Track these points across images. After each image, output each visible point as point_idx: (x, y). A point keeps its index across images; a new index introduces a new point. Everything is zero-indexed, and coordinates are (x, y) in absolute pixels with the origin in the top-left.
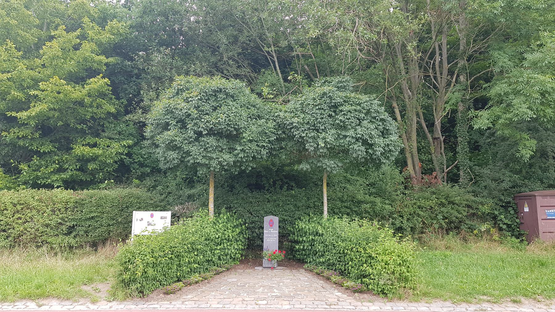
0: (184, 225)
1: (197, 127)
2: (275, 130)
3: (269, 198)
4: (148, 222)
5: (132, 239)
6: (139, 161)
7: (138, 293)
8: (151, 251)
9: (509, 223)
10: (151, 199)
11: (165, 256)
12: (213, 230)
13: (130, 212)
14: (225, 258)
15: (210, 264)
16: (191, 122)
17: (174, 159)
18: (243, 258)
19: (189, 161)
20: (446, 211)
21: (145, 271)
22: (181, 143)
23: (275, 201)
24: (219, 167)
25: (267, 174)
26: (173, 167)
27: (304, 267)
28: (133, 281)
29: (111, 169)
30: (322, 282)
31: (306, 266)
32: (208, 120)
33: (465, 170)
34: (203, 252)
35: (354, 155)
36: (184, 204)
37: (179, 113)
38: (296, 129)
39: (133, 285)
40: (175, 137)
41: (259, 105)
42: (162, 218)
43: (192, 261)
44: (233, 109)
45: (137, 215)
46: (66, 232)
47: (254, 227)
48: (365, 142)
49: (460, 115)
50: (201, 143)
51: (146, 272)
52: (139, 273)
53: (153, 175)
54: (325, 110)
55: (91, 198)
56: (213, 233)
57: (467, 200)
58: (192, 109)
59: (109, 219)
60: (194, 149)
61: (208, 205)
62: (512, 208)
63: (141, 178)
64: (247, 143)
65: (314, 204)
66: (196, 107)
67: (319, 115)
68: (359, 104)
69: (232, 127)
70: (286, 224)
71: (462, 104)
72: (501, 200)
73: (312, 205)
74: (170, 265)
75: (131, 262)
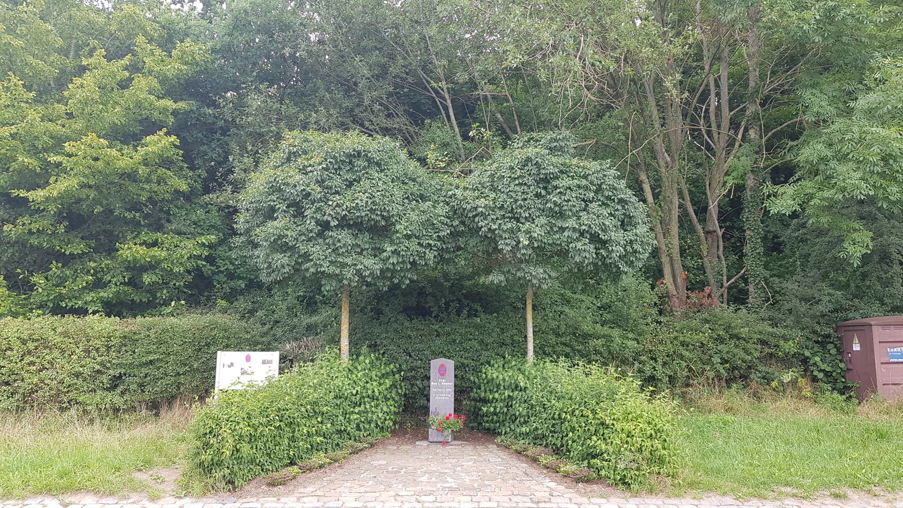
0: (301, 374)
1: (321, 213)
3: (439, 330)
4: (242, 369)
8: (247, 415)
10: (247, 332)
12: (347, 382)
13: (213, 354)
14: (367, 426)
15: (343, 437)
16: (311, 206)
17: (283, 267)
18: (397, 427)
19: (307, 270)
20: (726, 350)
21: (237, 449)
23: (449, 334)
26: (282, 279)
27: (496, 440)
28: (217, 464)
29: (182, 284)
30: (525, 465)
33: (758, 284)
34: (332, 418)
35: (577, 259)
36: (300, 339)
37: (292, 191)
38: (482, 218)
39: (218, 471)
40: (284, 231)
41: (422, 178)
42: (264, 362)
43: (314, 432)
45: (224, 358)
46: (109, 386)
47: (414, 377)
48: (595, 239)
50: (327, 241)
51: (238, 451)
52: (228, 452)
53: (250, 293)
54: (529, 187)
56: (347, 387)
58: (312, 184)
59: (177, 364)
60: (316, 250)
61: (339, 341)
63: (231, 297)
64: (403, 240)
66: (319, 182)
67: (520, 194)
68: (585, 177)
69: (377, 215)
70: (466, 371)
71: (752, 177)
72: (815, 332)
73: (508, 341)
74: (278, 438)
75: (213, 434)
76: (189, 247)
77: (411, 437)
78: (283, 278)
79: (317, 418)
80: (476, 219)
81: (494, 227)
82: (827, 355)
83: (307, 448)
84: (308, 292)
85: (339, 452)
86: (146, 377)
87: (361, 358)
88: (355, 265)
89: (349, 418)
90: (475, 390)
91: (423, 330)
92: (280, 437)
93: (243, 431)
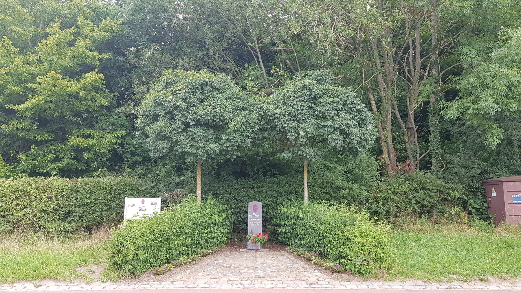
0: (173, 210)
1: (185, 118)
3: (254, 185)
4: (139, 208)
7: (130, 274)
8: (142, 234)
9: (478, 207)
10: (143, 186)
11: (155, 239)
14: (212, 241)
15: (198, 247)
17: (163, 149)
18: (229, 241)
19: (177, 150)
21: (136, 254)
22: (170, 133)
23: (259, 187)
26: (162, 155)
27: (286, 249)
28: (125, 263)
31: (288, 248)
32: (195, 111)
34: (191, 236)
36: (173, 191)
37: (168, 105)
38: (278, 120)
40: (164, 128)
43: (181, 244)
44: (219, 101)
45: (129, 201)
46: (62, 218)
48: (342, 132)
49: (432, 106)
50: (188, 133)
51: (137, 255)
52: (131, 256)
53: (144, 164)
54: (305, 102)
55: (85, 186)
57: (439, 186)
59: (102, 205)
60: (182, 139)
61: (195, 192)
63: (133, 166)
66: (184, 100)
70: (269, 209)
73: (293, 191)
74: (160, 248)
75: (123, 245)
78: (163, 155)
80: (275, 121)
81: (285, 125)
86: (84, 212)
87: (208, 201)
88: (205, 147)
93: (140, 243)
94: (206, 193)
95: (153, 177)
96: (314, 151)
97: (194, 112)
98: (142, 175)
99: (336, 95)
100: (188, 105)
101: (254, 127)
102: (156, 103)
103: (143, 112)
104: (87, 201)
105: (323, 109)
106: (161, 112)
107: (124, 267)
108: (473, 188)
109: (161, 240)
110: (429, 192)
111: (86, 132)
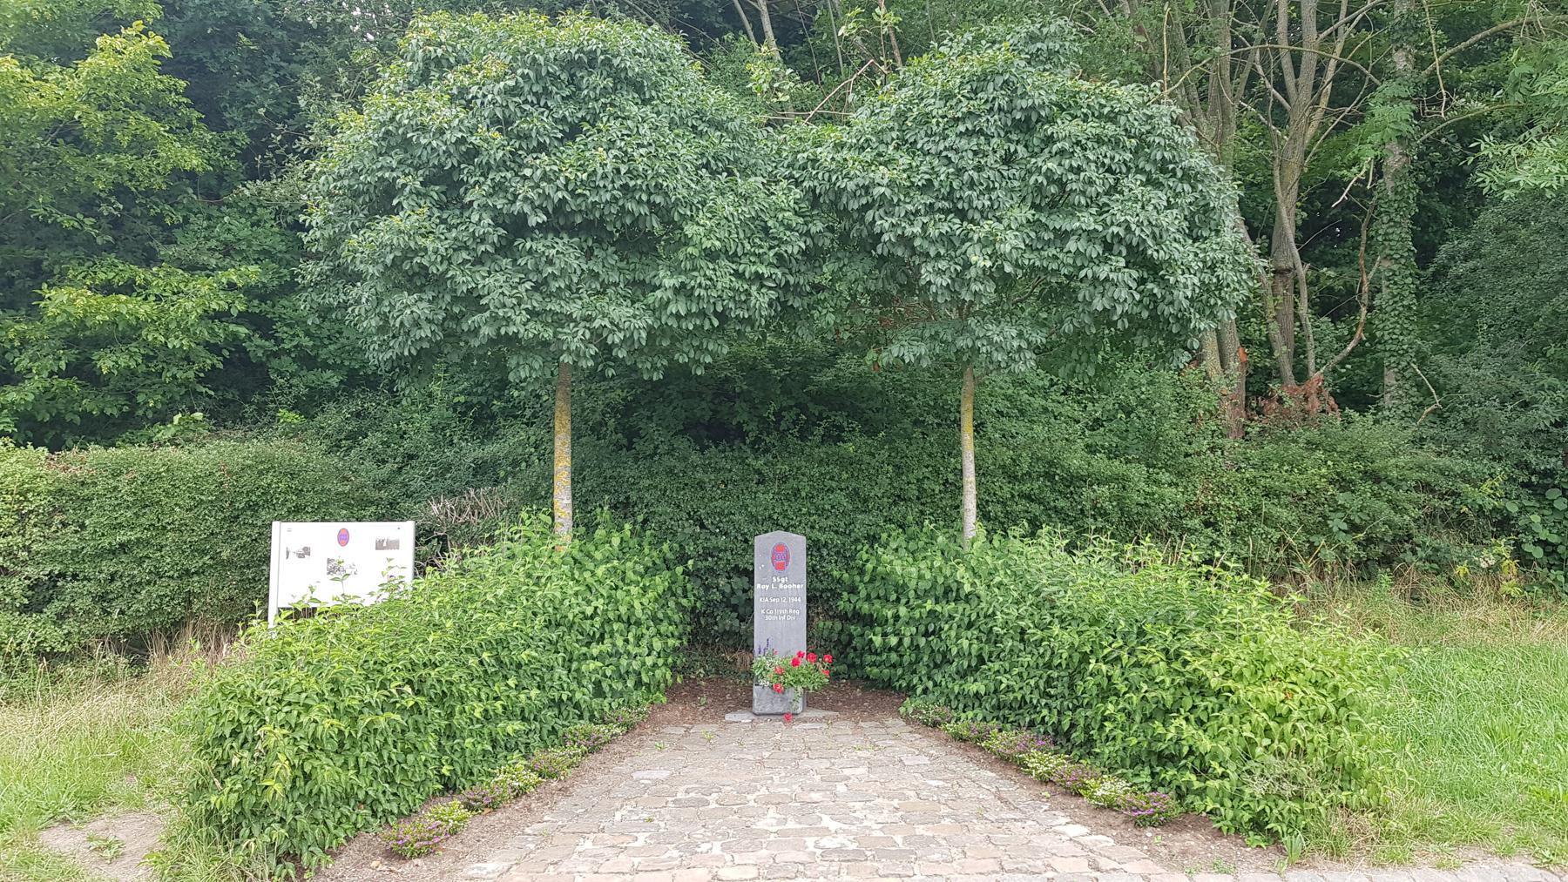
0: (463, 572)
1: (505, 197)
2: (801, 220)
3: (765, 470)
4: (329, 561)
5: (266, 630)
6: (296, 347)
7: (279, 862)
8: (331, 686)
9: (1554, 539)
10: (346, 479)
11: (389, 705)
12: (572, 588)
13: (264, 526)
14: (619, 686)
15: (565, 713)
16: (482, 179)
17: (417, 324)
18: (679, 680)
19: (475, 332)
20: (1357, 503)
21: (304, 773)
22: (446, 263)
23: (784, 479)
24: (593, 350)
25: (751, 389)
26: (414, 352)
27: (902, 710)
28: (253, 813)
29: (191, 374)
30: (990, 774)
31: (909, 705)
32: (548, 169)
33: (1404, 370)
34: (539, 673)
35: (1098, 304)
36: (461, 493)
37: (434, 143)
38: (881, 211)
39: (256, 832)
40: (418, 238)
41: (738, 121)
42: (380, 545)
43: (500, 710)
44: (642, 132)
45: (286, 536)
46: (26, 601)
47: (710, 570)
48: (1137, 257)
49: (1390, 185)
50: (521, 262)
51: (307, 777)
52: (278, 787)
53: (351, 396)
54: (988, 138)
55: (114, 476)
56: (573, 600)
57: (1421, 468)
58: (482, 128)
59: (184, 552)
60: (495, 283)
61: (550, 493)
62: (1557, 492)
63: (309, 405)
64: (703, 263)
65: (921, 490)
66: (499, 122)
67: (970, 155)
68: (1112, 118)
69: (640, 202)
70: (821, 556)
71: (1398, 150)
72: (1524, 465)
73: (913, 492)
74: (411, 735)
75: (242, 737)
76: (202, 294)
77: (710, 700)
78: (419, 352)
79: (506, 678)
80: (869, 216)
81: (909, 231)
82: (1546, 512)
83: (485, 752)
84: (476, 394)
85: (556, 753)
86: (112, 580)
87: (600, 533)
88: (589, 319)
89: (577, 671)
90: (845, 594)
91: (730, 471)
92: (418, 730)
93: (320, 729)
94: (586, 503)
95: (383, 443)
96: (1020, 335)
97: (545, 173)
98: (346, 439)
99: (1106, 110)
100: (517, 145)
101: (786, 242)
102: (384, 139)
103: (330, 179)
104: (121, 537)
105: (1060, 165)
106: (406, 175)
107: (251, 836)
108: (1534, 472)
109: (416, 703)
110: (1389, 487)
111: (121, 271)
